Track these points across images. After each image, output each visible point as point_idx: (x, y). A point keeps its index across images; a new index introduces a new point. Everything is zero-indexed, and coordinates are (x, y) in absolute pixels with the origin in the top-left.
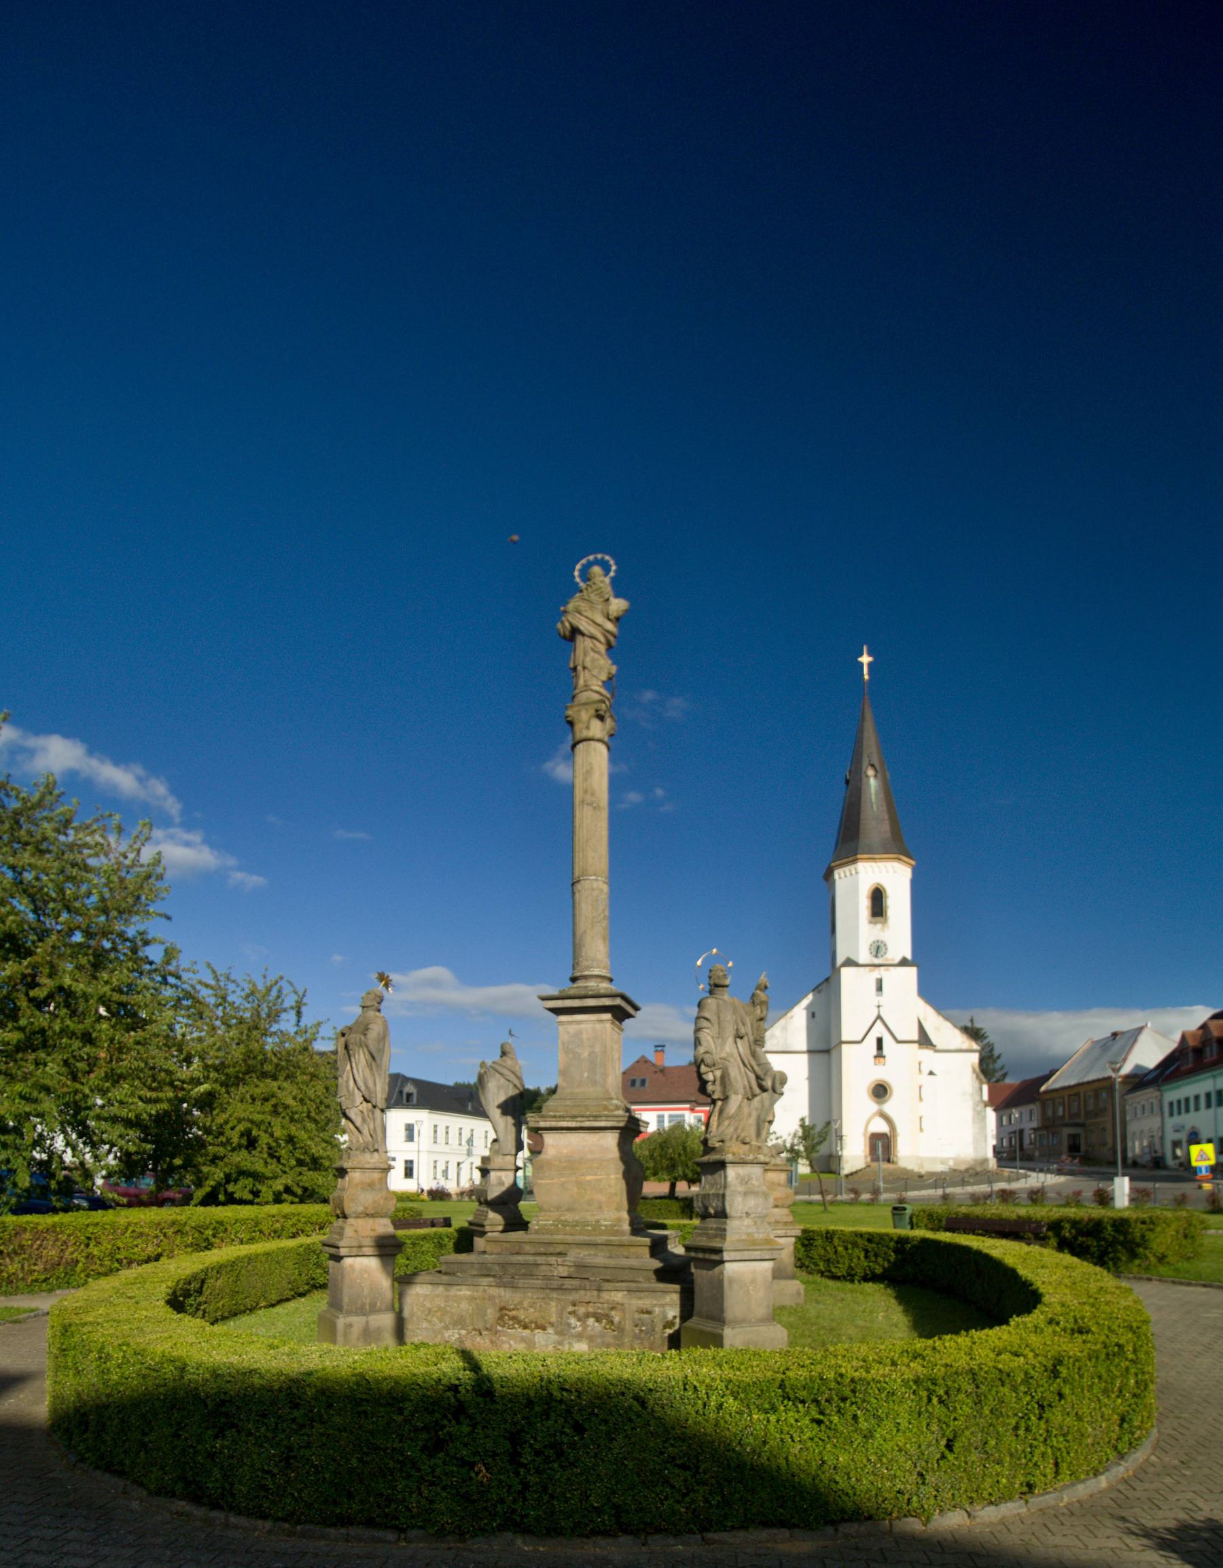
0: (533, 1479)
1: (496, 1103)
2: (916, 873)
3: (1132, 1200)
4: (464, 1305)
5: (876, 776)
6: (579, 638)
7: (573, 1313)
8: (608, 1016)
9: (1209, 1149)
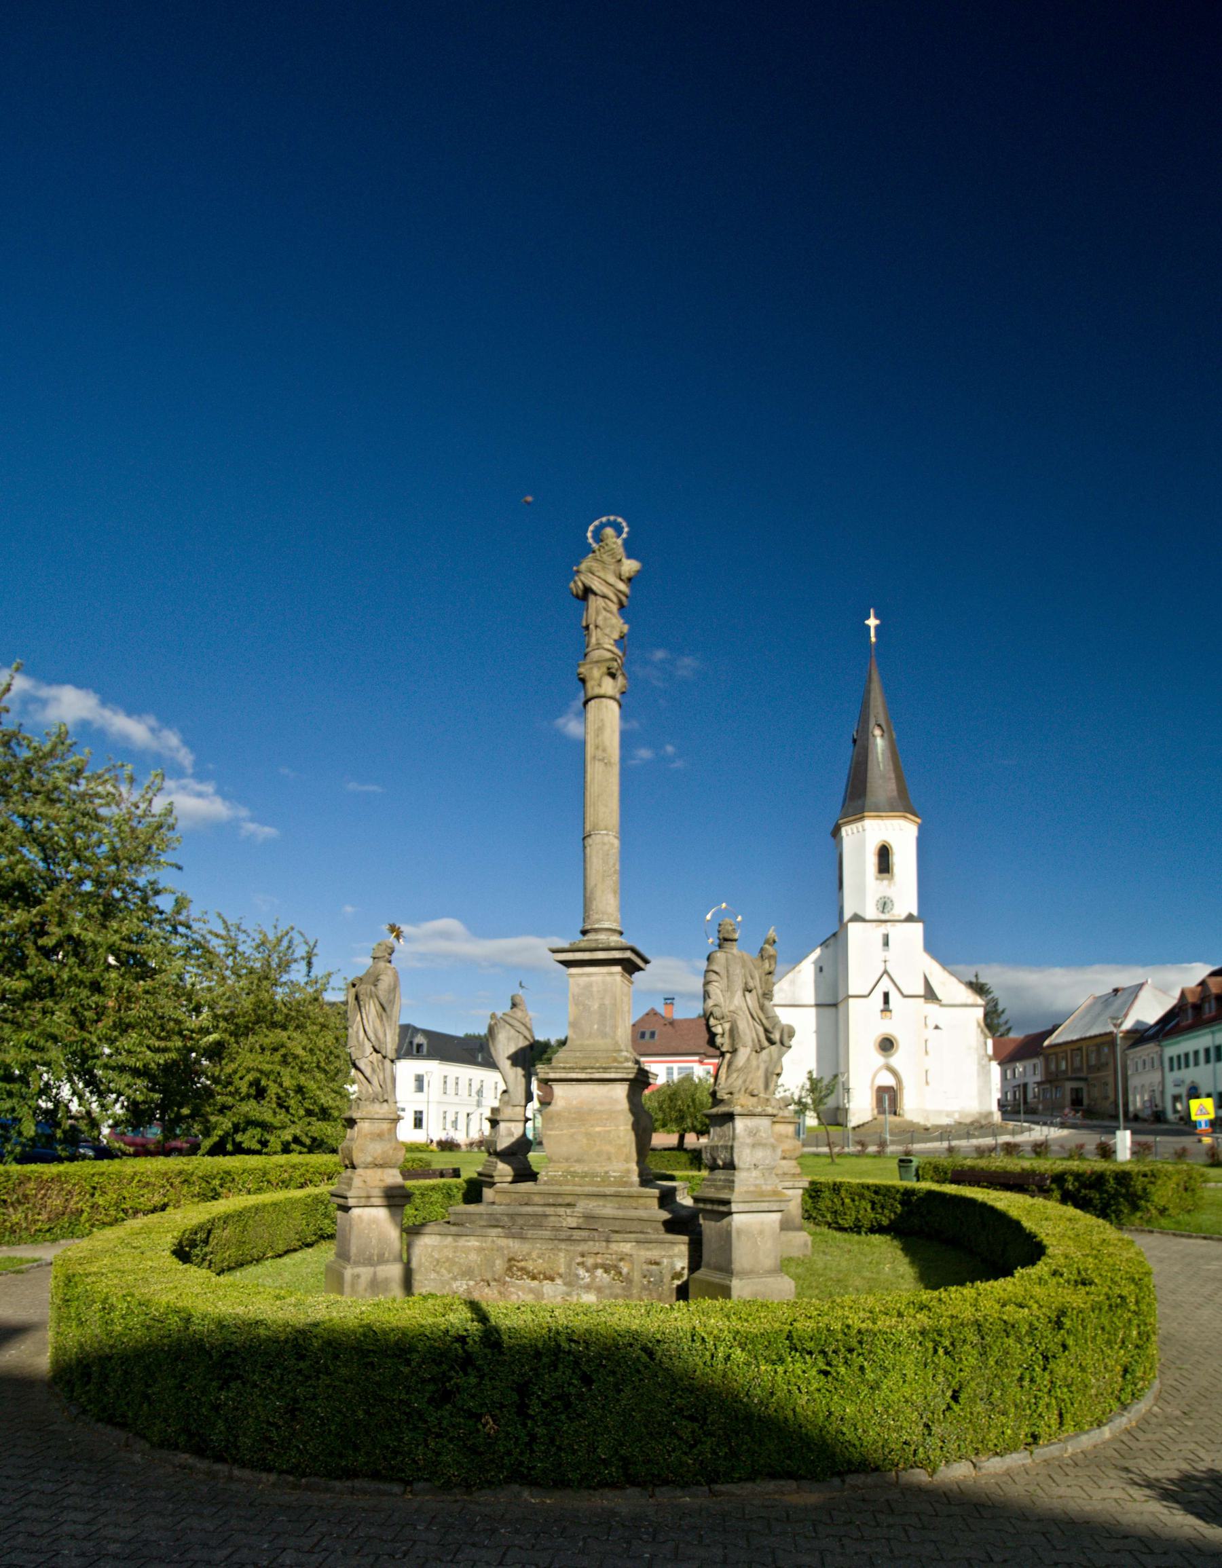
0: (541, 1431)
1: (507, 1055)
2: (921, 829)
3: (1133, 1153)
4: (473, 1256)
5: (882, 736)
6: (592, 598)
7: (582, 1264)
8: (618, 969)
9: (1209, 1103)
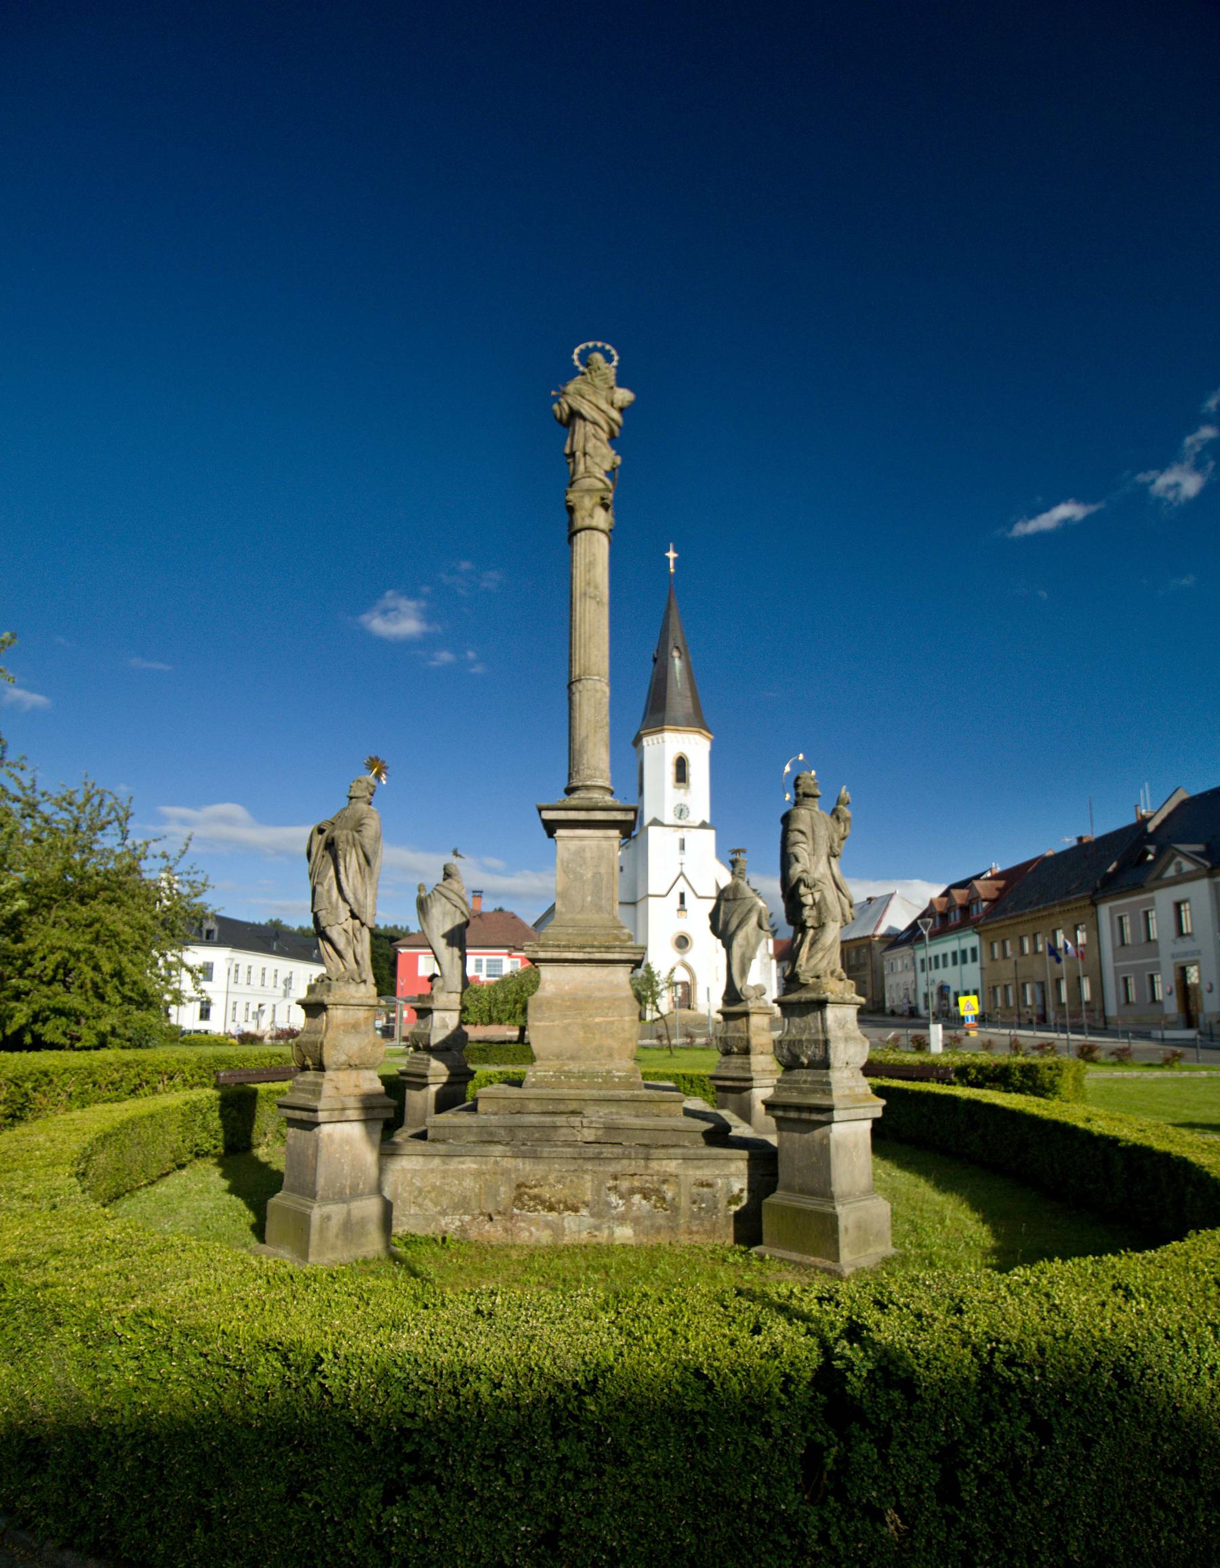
0: (979, 1526)
1: (442, 933)
2: (714, 745)
3: (945, 1046)
4: (468, 1182)
6: (579, 424)
7: (614, 1189)
8: (615, 833)
9: (973, 999)
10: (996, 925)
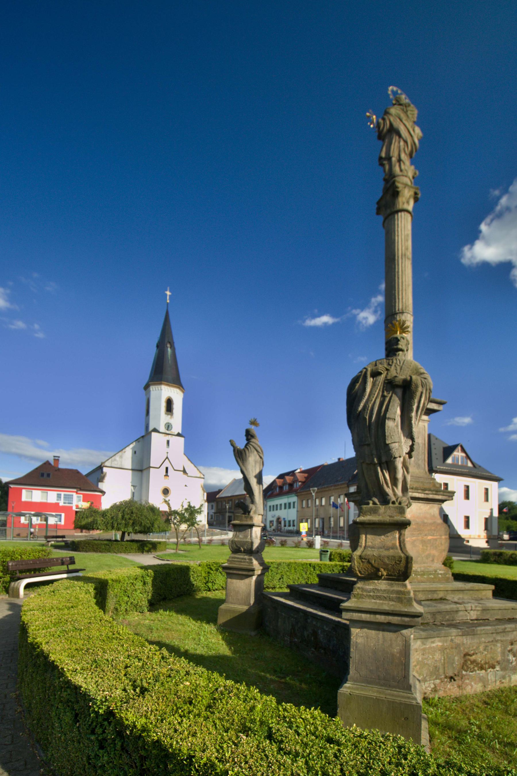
1: (254, 474)
6: (395, 138)
10: (305, 493)
